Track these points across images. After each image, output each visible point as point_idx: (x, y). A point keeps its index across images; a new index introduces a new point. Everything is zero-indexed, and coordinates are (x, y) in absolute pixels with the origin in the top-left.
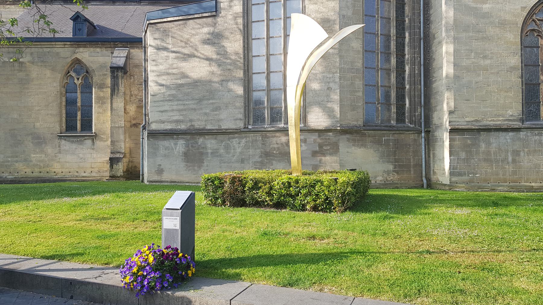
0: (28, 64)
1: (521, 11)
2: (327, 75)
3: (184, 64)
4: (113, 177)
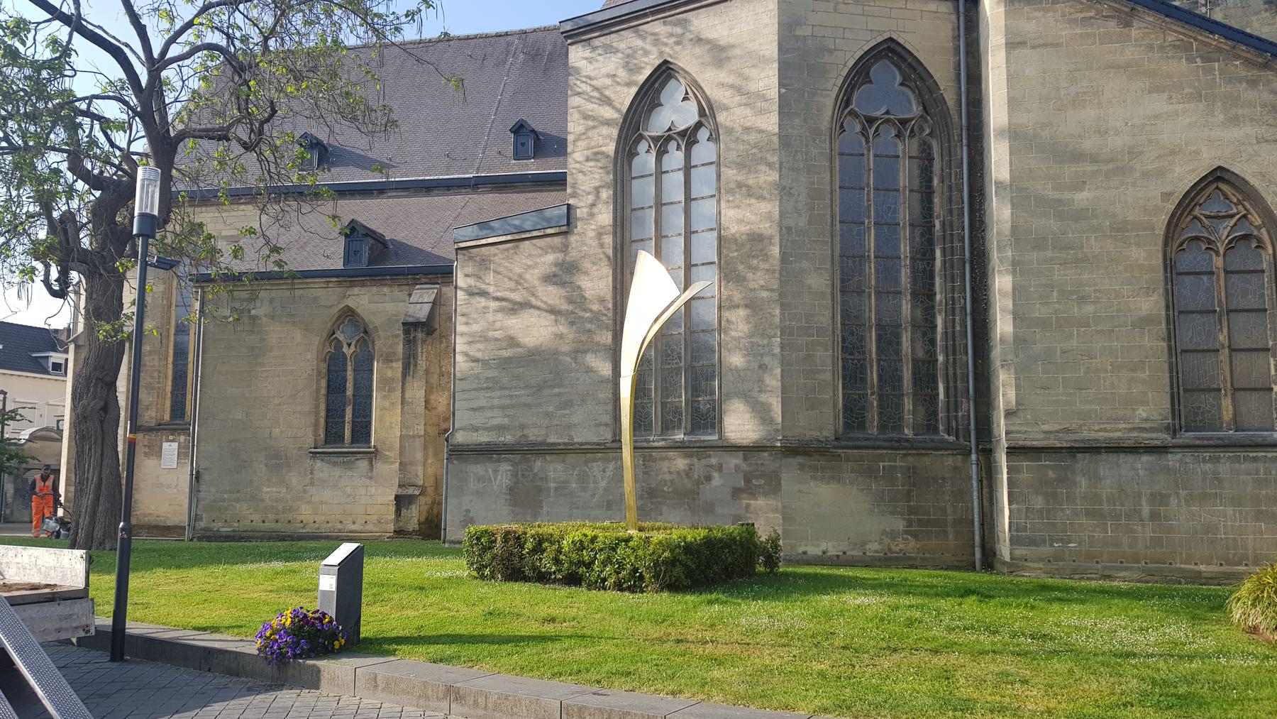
0: (264, 318)
1: (1163, 201)
2: (759, 340)
3: (514, 321)
4: (399, 533)
